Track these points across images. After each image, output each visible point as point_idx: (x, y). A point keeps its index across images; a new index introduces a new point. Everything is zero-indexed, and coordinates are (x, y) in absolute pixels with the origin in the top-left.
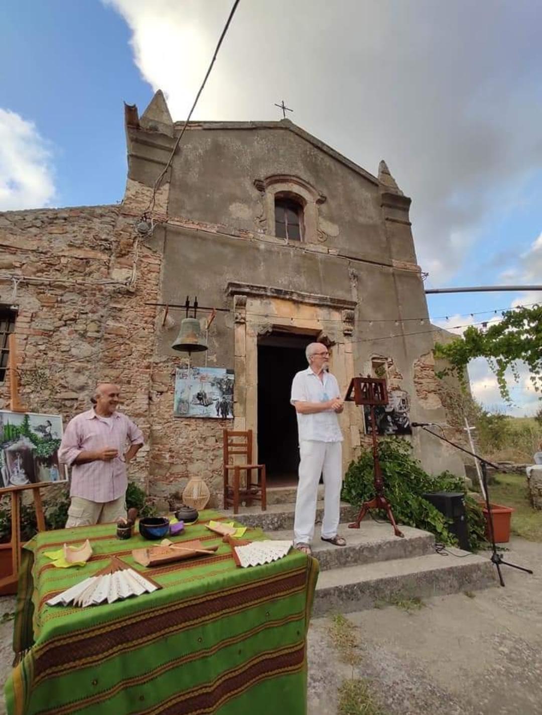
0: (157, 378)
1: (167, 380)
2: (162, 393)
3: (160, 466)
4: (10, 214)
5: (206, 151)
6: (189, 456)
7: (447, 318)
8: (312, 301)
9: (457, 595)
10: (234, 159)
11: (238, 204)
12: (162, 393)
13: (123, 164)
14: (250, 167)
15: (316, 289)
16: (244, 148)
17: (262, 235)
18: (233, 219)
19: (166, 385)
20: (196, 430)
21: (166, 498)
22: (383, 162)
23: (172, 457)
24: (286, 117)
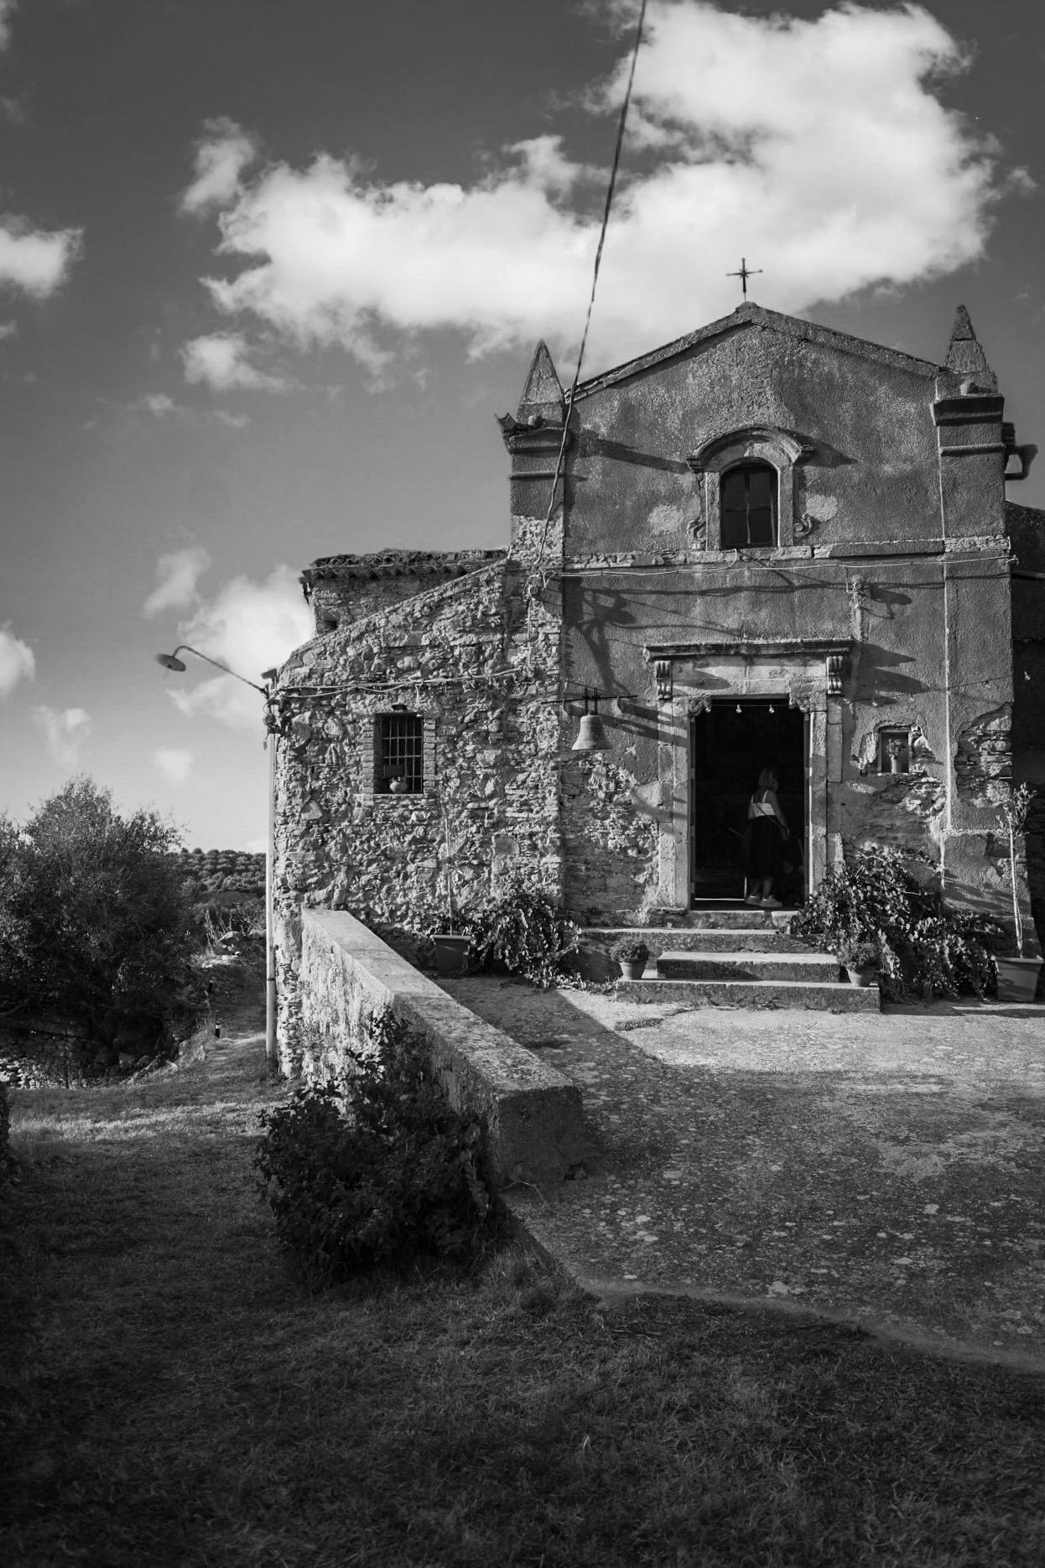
0: (567, 779)
1: (579, 781)
2: (574, 796)
3: (576, 878)
4: (435, 969)
5: (612, 427)
6: (607, 868)
7: (172, 663)
8: (771, 652)
9: (883, 1018)
10: (654, 424)
11: (662, 508)
12: (574, 796)
13: (504, 492)
14: (680, 430)
15: (787, 627)
16: (671, 397)
17: (698, 554)
18: (654, 537)
19: (577, 787)
20: (997, 1191)
21: (582, 912)
22: (962, 309)
23: (587, 869)
24: (751, 299)
